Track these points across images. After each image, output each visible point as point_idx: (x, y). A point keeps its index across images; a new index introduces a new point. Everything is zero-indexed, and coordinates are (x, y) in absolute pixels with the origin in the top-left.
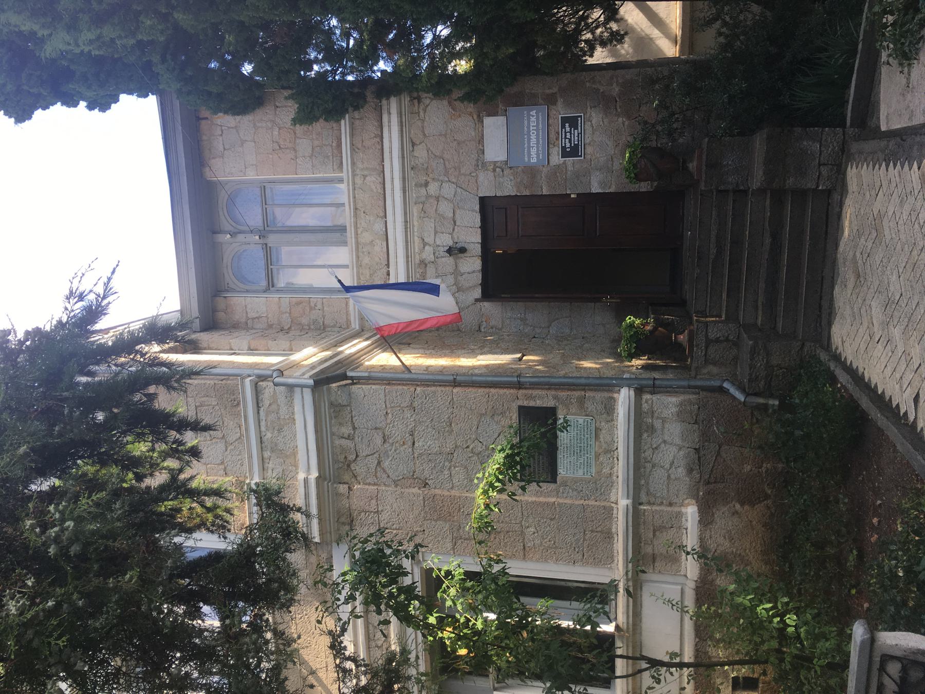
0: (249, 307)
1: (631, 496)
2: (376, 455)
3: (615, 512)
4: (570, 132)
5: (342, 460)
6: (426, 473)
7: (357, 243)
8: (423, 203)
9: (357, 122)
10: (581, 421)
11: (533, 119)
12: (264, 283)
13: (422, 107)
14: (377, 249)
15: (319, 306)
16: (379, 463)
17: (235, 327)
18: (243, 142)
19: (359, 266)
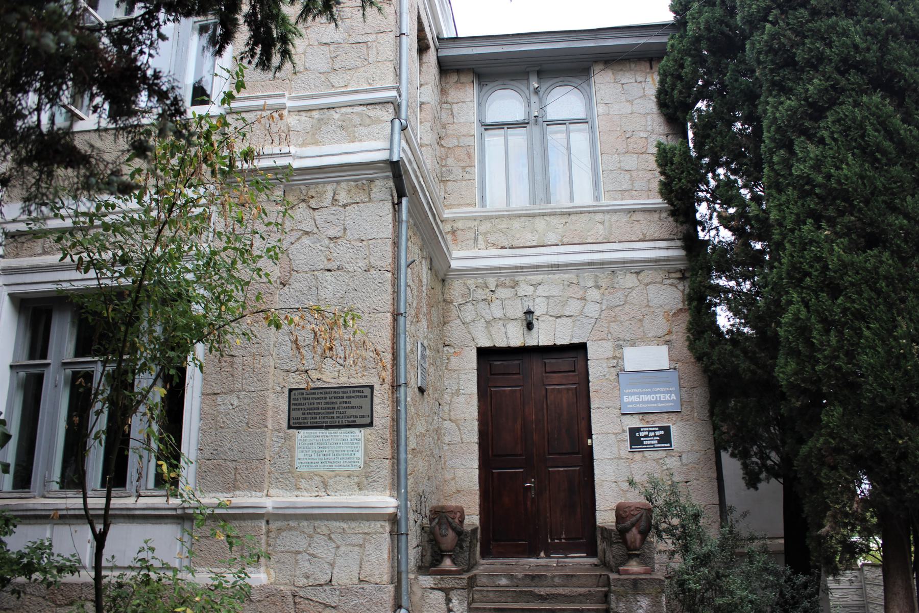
0: (464, 105)
1: (276, 511)
2: (315, 230)
3: (259, 494)
4: (655, 436)
5: (310, 194)
6: (296, 285)
7: (534, 216)
8: (578, 284)
9: (656, 216)
10: (358, 455)
11: (667, 397)
12: (489, 120)
13: (675, 281)
14: (529, 236)
15: (466, 176)
16: (307, 233)
17: (443, 92)
18: (631, 102)
19: (510, 217)
